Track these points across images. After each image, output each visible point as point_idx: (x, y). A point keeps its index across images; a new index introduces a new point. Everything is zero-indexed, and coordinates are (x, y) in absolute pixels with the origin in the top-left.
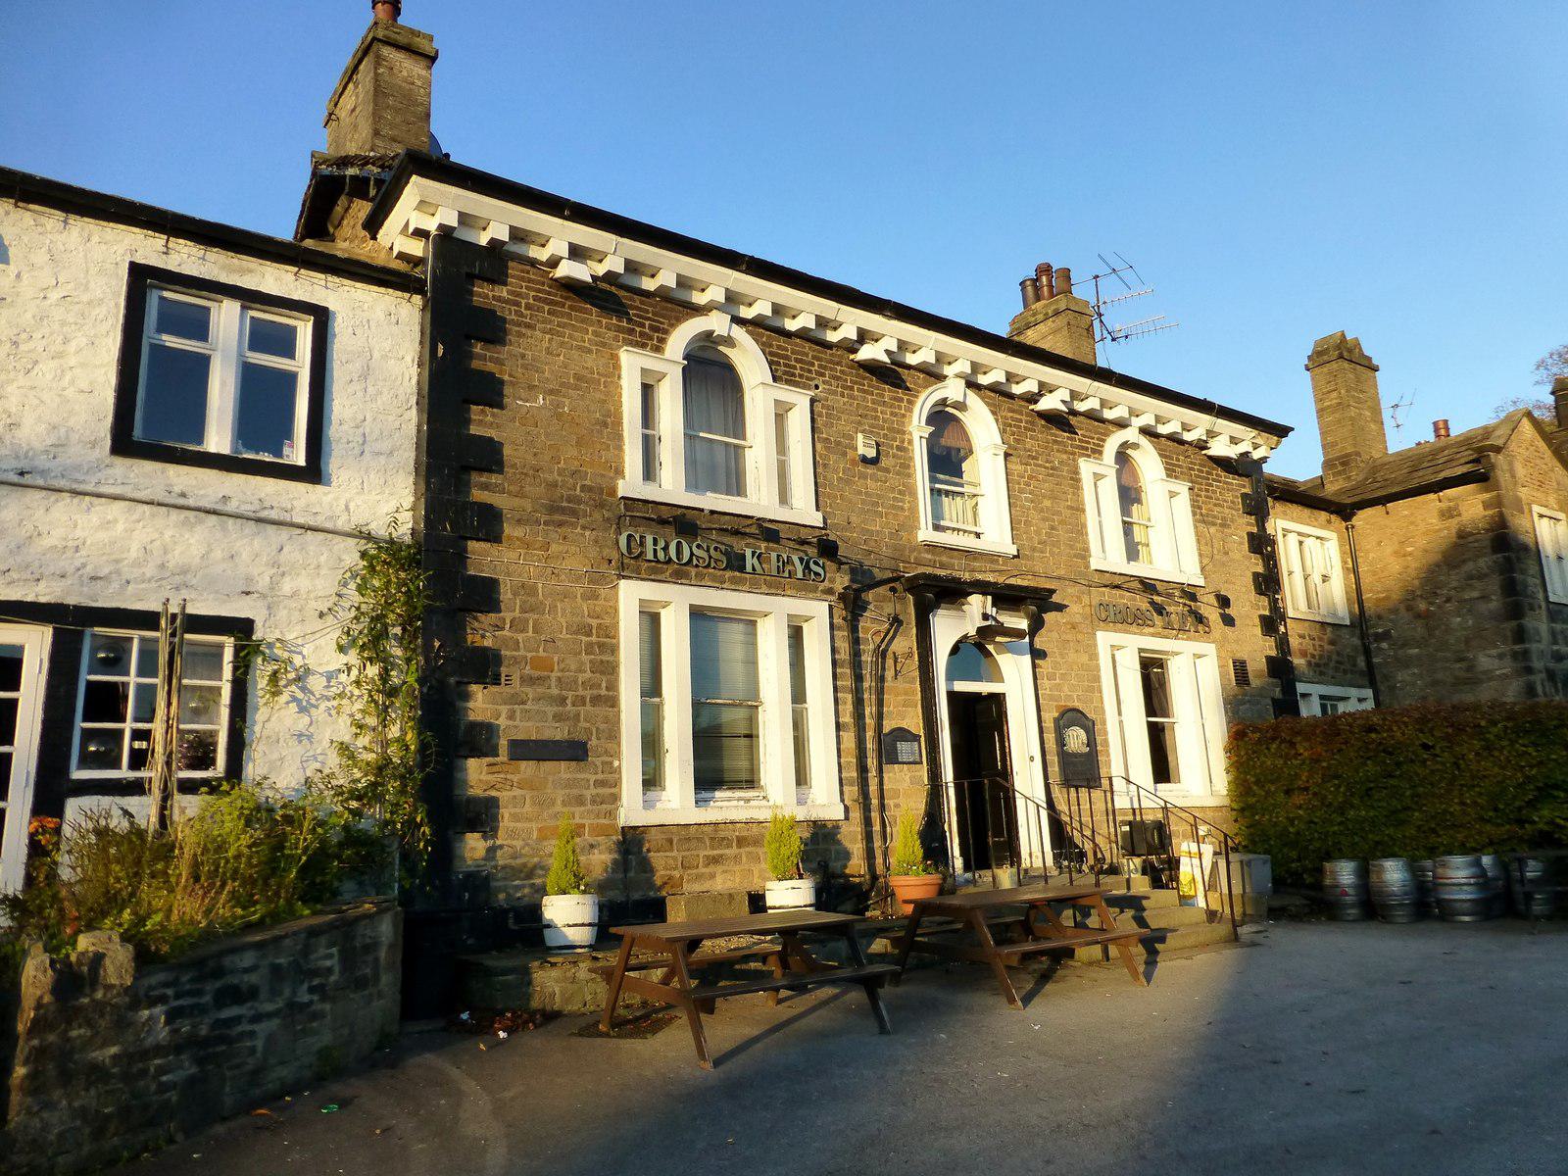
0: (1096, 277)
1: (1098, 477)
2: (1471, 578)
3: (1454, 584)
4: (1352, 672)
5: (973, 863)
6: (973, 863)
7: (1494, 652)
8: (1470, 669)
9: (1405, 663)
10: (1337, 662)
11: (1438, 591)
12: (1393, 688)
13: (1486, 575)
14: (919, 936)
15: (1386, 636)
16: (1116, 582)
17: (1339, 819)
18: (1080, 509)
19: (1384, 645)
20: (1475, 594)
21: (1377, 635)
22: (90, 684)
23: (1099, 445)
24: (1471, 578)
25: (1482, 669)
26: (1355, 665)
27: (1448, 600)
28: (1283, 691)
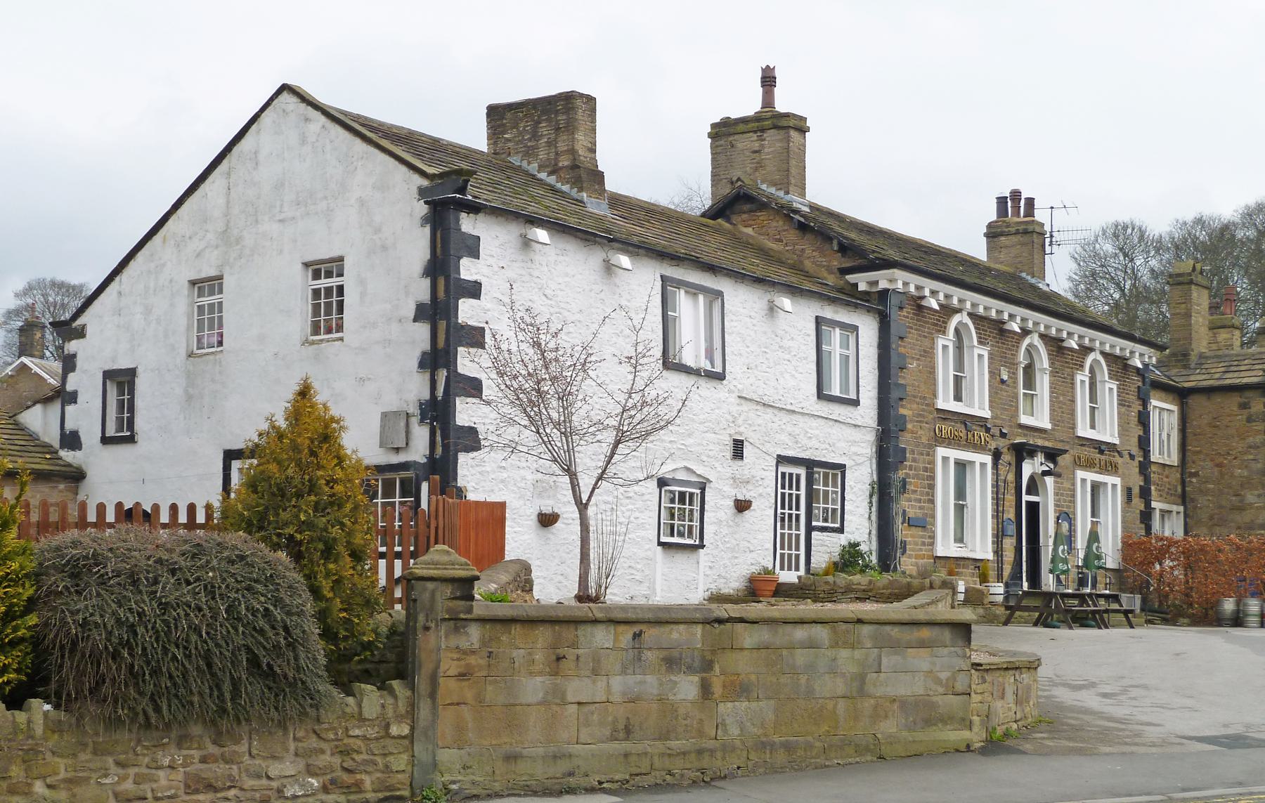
0: (1052, 254)
1: (945, 347)
2: (1250, 447)
3: (1240, 449)
4: (1175, 495)
5: (1024, 575)
6: (1024, 575)
7: (1256, 492)
8: (1241, 501)
9: (1203, 492)
10: (1169, 489)
11: (1231, 452)
12: (1195, 508)
13: (1258, 447)
14: (1035, 609)
15: (1196, 475)
16: (946, 415)
17: (609, 513)
18: (1073, 401)
19: (1194, 480)
20: (1251, 457)
21: (1191, 473)
22: (1027, 502)
23: (1081, 362)
24: (1250, 447)
25: (1248, 502)
26: (1176, 491)
27: (1235, 458)
28: (1145, 507)
